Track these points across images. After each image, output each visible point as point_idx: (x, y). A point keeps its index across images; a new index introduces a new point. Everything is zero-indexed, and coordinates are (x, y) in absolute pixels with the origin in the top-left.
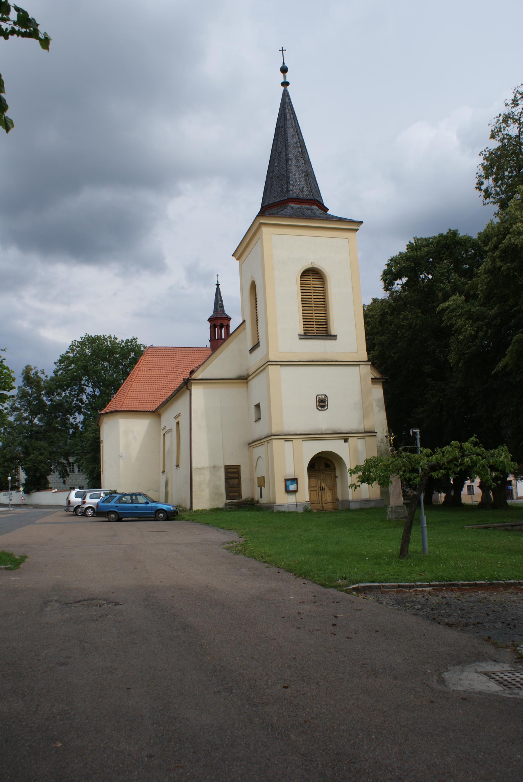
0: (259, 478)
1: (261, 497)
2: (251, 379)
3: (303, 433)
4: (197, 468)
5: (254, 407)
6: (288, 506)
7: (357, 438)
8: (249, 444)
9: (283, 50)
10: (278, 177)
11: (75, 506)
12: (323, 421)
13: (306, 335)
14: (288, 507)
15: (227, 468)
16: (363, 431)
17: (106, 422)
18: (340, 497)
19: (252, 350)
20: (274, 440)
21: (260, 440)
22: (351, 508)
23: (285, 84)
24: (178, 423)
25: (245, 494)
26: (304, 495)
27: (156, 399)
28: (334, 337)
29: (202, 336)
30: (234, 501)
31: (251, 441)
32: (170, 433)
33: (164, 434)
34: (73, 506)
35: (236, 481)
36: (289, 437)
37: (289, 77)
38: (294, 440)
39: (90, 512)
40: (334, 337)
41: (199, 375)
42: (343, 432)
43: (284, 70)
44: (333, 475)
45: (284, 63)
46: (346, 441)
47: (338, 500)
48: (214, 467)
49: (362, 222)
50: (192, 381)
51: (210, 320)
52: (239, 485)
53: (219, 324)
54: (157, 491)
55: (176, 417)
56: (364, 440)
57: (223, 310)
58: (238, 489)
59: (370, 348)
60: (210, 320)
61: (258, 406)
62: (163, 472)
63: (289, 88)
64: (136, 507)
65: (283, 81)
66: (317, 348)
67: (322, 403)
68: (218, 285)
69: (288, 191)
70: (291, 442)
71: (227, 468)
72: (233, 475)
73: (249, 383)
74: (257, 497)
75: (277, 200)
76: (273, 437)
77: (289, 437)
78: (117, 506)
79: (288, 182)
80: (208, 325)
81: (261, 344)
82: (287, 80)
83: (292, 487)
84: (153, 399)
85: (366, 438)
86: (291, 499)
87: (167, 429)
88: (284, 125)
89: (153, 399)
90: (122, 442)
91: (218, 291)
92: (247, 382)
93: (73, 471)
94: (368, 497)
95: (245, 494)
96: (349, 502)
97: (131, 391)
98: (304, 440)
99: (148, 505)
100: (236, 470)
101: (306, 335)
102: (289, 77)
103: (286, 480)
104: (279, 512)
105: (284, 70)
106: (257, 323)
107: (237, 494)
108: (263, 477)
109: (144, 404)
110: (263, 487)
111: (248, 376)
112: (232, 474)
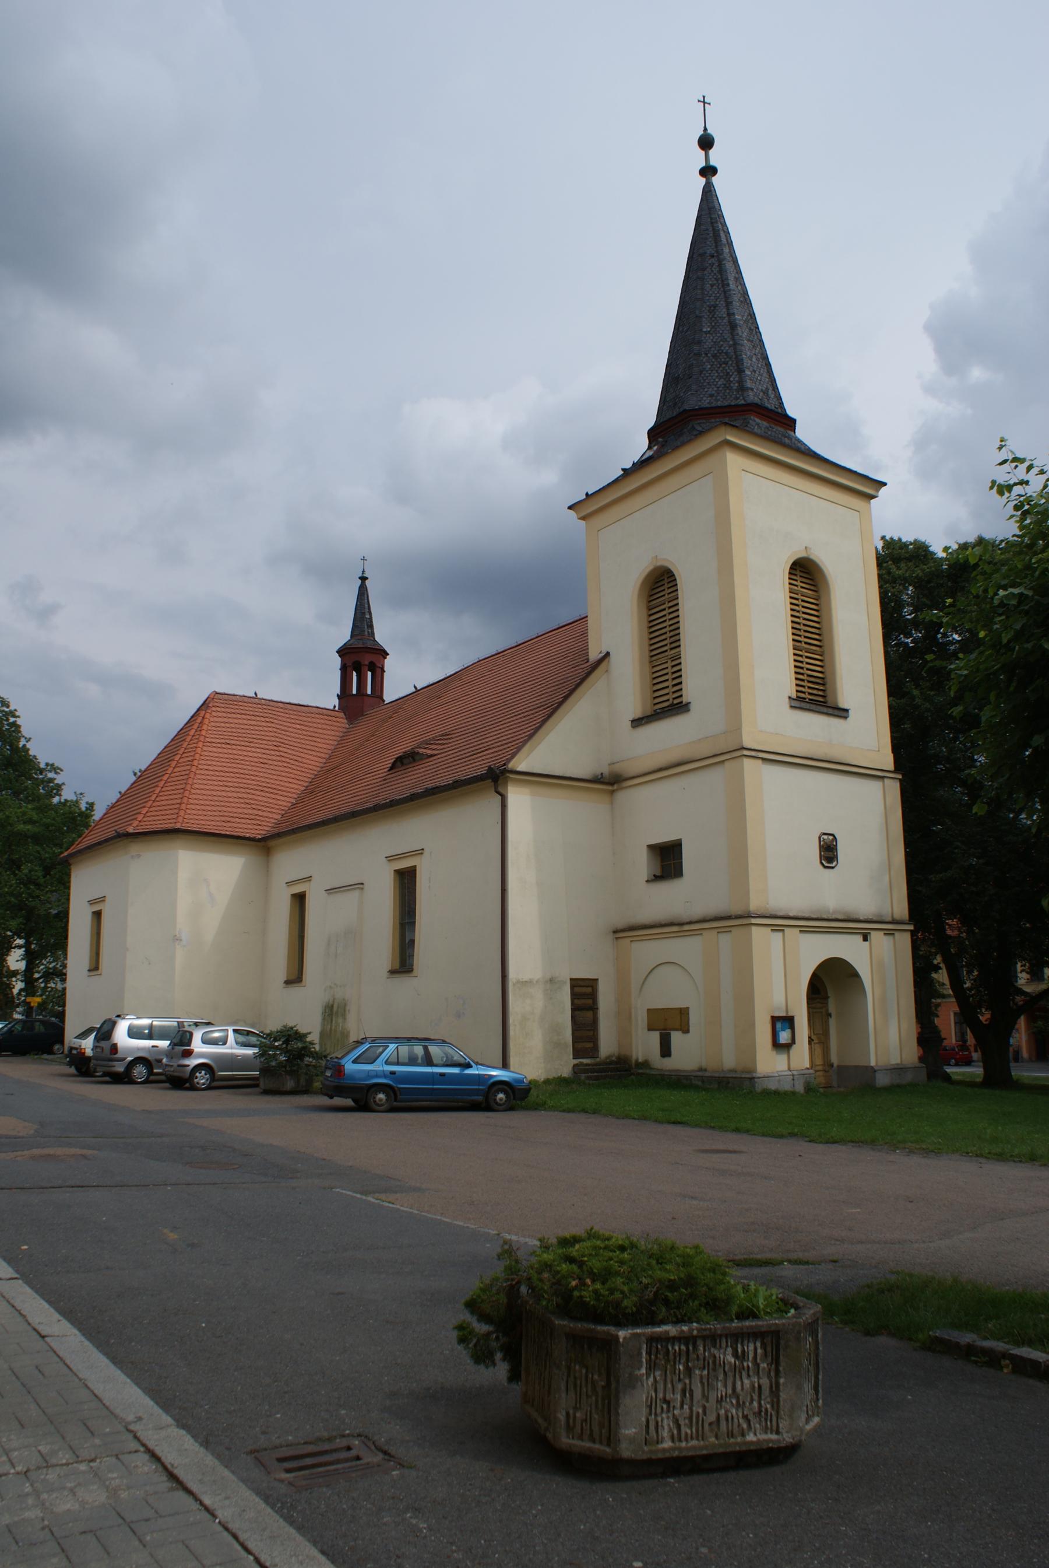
3: (800, 914)
4: (518, 982)
5: (645, 850)
7: (882, 933)
8: (615, 932)
9: (704, 103)
10: (714, 356)
11: (130, 1059)
14: (779, 1081)
15: (575, 983)
16: (889, 919)
17: (139, 856)
18: (834, 1060)
20: (754, 928)
21: (681, 924)
22: (877, 1085)
23: (708, 171)
25: (607, 1045)
26: (801, 1056)
27: (256, 812)
28: (842, 713)
30: (585, 1061)
34: (123, 1059)
35: (590, 1014)
36: (780, 921)
37: (716, 157)
38: (787, 930)
39: (202, 1078)
40: (842, 713)
41: (522, 763)
42: (861, 918)
43: (706, 143)
45: (705, 129)
47: (832, 1065)
48: (552, 980)
49: (885, 484)
50: (511, 776)
51: (341, 652)
52: (595, 1022)
53: (367, 663)
56: (891, 938)
57: (373, 634)
59: (898, 746)
60: (341, 652)
63: (715, 180)
64: (442, 1075)
65: (703, 164)
67: (829, 852)
68: (363, 579)
69: (742, 388)
70: (780, 934)
71: (575, 983)
72: (583, 1001)
75: (719, 404)
76: (754, 921)
77: (780, 921)
78: (393, 1073)
79: (740, 371)
82: (712, 163)
83: (784, 1037)
84: (251, 811)
85: (897, 934)
88: (717, 252)
89: (251, 811)
90: (184, 901)
92: (612, 792)
94: (899, 1061)
95: (607, 1045)
96: (873, 1070)
98: (805, 930)
99: (468, 1071)
100: (589, 990)
102: (716, 157)
104: (767, 1093)
105: (706, 143)
112: (584, 995)
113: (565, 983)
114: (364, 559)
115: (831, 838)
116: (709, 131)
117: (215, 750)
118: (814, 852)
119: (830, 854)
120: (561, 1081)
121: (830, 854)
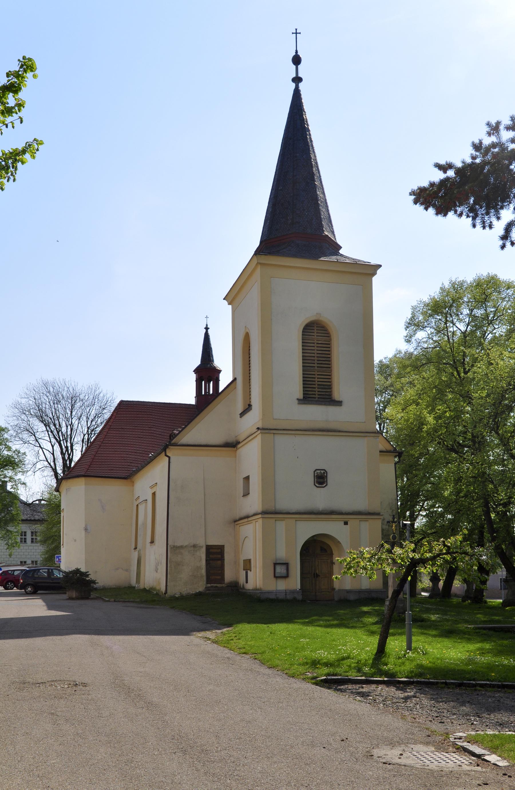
0: (245, 561)
1: (247, 582)
2: (241, 447)
4: (174, 546)
6: (277, 592)
12: (321, 498)
13: (307, 398)
15: (209, 548)
19: (242, 414)
23: (297, 80)
24: (154, 494)
25: (229, 576)
28: (339, 403)
29: (187, 395)
31: (237, 518)
32: (144, 504)
33: (137, 505)
40: (339, 403)
42: (344, 512)
43: (297, 60)
44: (329, 561)
45: (297, 52)
46: (346, 523)
47: (334, 589)
49: (380, 266)
54: (127, 570)
55: (152, 487)
58: (220, 572)
61: (247, 478)
62: (136, 548)
65: (295, 76)
66: (316, 414)
67: (321, 479)
68: (207, 328)
71: (209, 548)
73: (238, 451)
74: (242, 580)
80: (194, 377)
81: (253, 407)
82: (300, 75)
86: (282, 586)
87: (141, 500)
91: (207, 338)
93: (25, 542)
94: (368, 587)
97: (99, 452)
100: (220, 550)
101: (307, 398)
103: (275, 564)
105: (297, 60)
106: (250, 382)
107: (219, 577)
108: (250, 560)
109: (115, 469)
110: (249, 571)
111: (238, 443)
113: (202, 547)
114: (207, 317)
115: (322, 472)
116: (299, 54)
117: (114, 432)
118: (310, 479)
119: (321, 480)
120: (199, 595)
121: (321, 480)
